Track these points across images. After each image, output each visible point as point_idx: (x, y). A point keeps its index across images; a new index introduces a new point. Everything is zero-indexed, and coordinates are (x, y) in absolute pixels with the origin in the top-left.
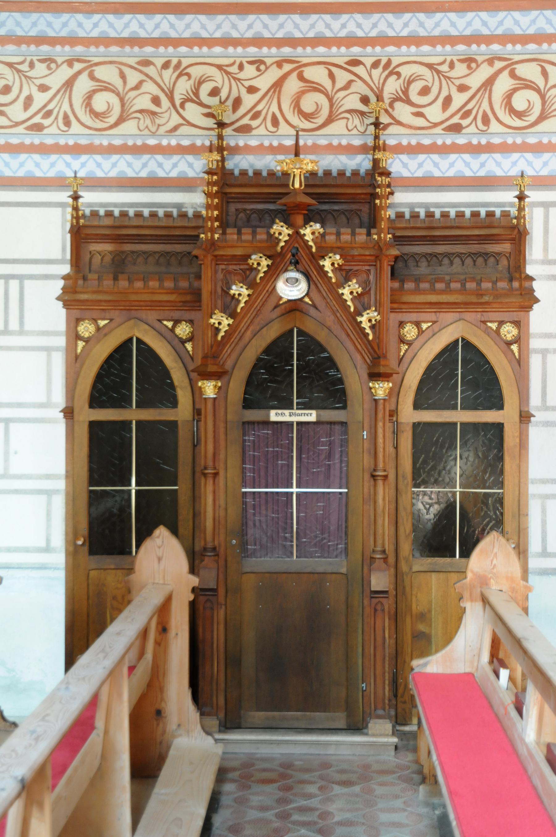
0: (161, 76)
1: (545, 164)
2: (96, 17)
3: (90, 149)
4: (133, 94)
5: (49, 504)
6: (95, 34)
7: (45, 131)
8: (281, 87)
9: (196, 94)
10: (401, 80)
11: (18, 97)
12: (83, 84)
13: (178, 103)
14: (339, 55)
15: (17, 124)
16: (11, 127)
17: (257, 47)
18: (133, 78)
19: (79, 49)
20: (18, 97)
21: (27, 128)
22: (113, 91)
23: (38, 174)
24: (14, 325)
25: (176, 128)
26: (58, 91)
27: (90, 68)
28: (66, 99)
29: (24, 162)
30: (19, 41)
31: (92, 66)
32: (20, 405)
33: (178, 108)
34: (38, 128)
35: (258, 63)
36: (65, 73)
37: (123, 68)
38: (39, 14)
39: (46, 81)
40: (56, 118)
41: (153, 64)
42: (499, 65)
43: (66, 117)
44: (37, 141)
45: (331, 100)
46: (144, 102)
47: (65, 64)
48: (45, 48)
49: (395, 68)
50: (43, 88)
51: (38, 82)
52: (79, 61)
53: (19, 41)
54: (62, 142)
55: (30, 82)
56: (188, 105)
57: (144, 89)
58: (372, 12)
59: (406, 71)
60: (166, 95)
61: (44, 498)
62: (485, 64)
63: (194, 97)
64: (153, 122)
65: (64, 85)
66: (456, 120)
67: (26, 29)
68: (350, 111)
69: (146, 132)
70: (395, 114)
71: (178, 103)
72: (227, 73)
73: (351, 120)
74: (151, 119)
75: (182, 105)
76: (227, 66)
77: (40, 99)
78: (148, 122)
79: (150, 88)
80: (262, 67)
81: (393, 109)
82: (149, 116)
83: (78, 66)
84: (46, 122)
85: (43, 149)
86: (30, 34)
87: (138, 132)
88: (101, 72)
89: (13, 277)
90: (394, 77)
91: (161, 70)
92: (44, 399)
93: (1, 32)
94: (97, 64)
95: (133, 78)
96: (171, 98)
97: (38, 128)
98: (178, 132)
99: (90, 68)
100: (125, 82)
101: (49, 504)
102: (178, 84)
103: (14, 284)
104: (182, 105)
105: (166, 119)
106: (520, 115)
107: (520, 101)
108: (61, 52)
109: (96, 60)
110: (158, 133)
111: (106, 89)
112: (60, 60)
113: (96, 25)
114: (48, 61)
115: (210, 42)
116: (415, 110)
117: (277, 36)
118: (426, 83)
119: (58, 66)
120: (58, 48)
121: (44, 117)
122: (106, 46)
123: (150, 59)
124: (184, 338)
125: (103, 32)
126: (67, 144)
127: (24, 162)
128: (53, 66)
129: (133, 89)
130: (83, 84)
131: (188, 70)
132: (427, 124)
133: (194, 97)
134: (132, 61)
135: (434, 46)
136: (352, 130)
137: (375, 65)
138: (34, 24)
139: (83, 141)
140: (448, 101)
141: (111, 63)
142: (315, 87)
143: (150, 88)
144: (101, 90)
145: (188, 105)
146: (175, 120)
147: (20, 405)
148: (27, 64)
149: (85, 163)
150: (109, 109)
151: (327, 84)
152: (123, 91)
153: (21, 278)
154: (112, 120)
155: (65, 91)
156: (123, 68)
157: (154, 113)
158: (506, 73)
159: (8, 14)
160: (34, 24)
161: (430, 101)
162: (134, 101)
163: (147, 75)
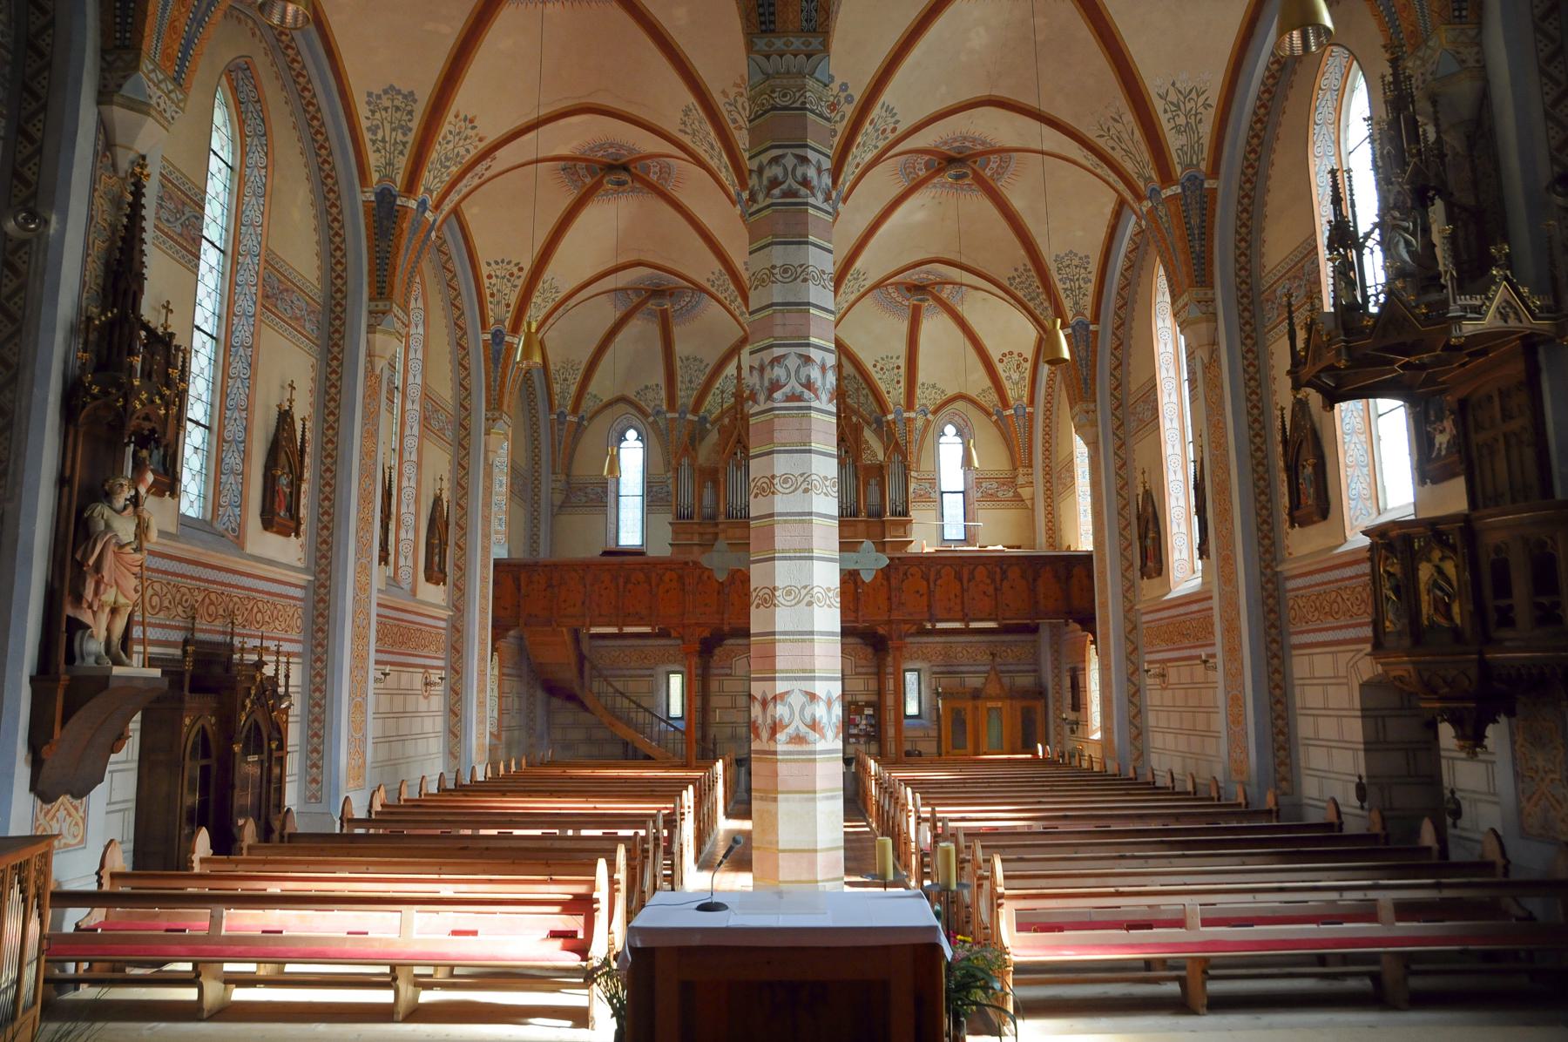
14: (220, 588)
142: (212, 603)
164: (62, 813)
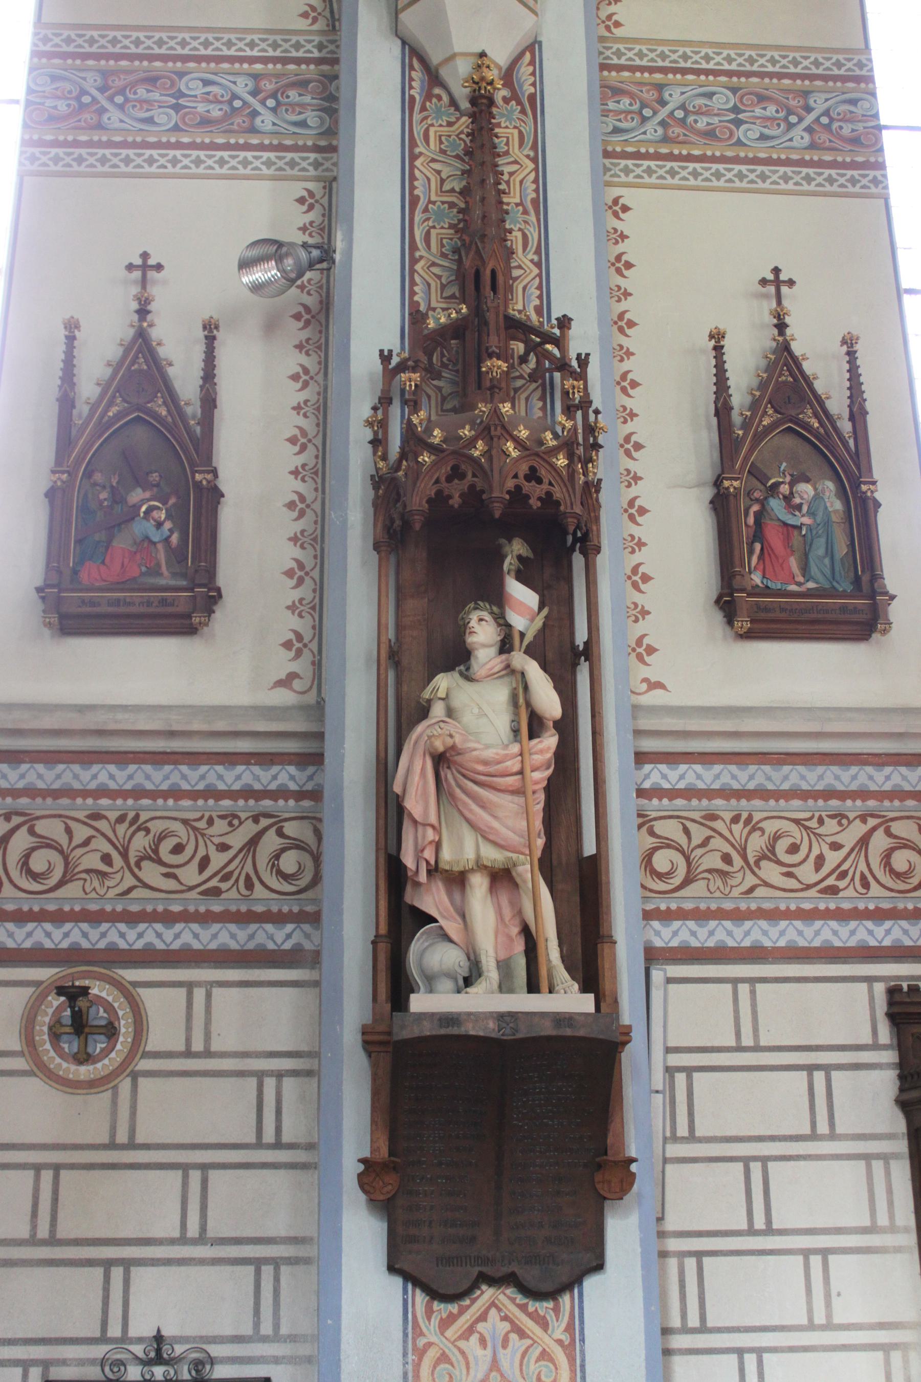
0: (114, 831)
2: (888, 770)
3: (893, 914)
5: (887, 1363)
6: (888, 787)
7: (841, 894)
8: (7, 843)
9: (156, 851)
10: (151, 836)
11: (808, 856)
12: (879, 842)
13: (752, 861)
15: (809, 887)
16: (802, 890)
18: (81, 833)
19: (871, 803)
20: (808, 856)
21: (820, 892)
22: (56, 849)
24: (823, 1128)
25: (751, 890)
26: (852, 850)
27: (886, 824)
28: (862, 858)
29: (819, 930)
30: (805, 795)
31: (887, 821)
32: (838, 1231)
33: (134, 867)
34: (833, 891)
35: (231, 818)
36: (858, 830)
37: (69, 822)
38: (825, 767)
39: (838, 839)
40: (853, 879)
41: (106, 818)
42: (16, 820)
43: (248, 877)
44: (832, 906)
45: (66, 859)
46: (93, 861)
47: (858, 820)
48: (834, 803)
49: (758, 823)
50: (836, 846)
51: (829, 840)
52: (872, 816)
53: (805, 795)
54: (861, 906)
55: (208, 842)
56: (763, 863)
57: (94, 845)
58: (712, 763)
59: (157, 827)
60: (738, 852)
61: (880, 1355)
62: (858, 821)
63: (769, 854)
64: (725, 883)
65: (858, 842)
66: (214, 883)
67: (812, 783)
70: (760, 873)
71: (132, 861)
72: (807, 828)
73: (712, 881)
75: (757, 863)
76: (195, 820)
77: (833, 858)
78: (719, 883)
79: (717, 843)
80: (844, 821)
81: (140, 868)
83: (872, 822)
84: (842, 884)
85: (841, 915)
86: (817, 788)
87: (83, 895)
88: (41, 827)
89: (818, 1067)
90: (143, 833)
92: (867, 1223)
95: (81, 833)
96: (125, 855)
97: (833, 891)
98: (131, 895)
99: (886, 824)
100: (71, 839)
101: (887, 1363)
102: (133, 841)
103: (819, 1076)
104: (757, 863)
105: (740, 879)
106: (35, 876)
107: (38, 863)
108: (853, 807)
109: (892, 815)
110: (107, 896)
111: (905, 846)
112: (851, 816)
113: (888, 778)
114: (839, 816)
115: (778, 795)
116: (165, 870)
117: (161, 788)
118: (178, 840)
119: (850, 822)
120: (849, 803)
121: (838, 879)
122: (902, 800)
123: (104, 813)
125: (895, 785)
126: (238, 911)
127: (819, 930)
128: (844, 821)
129: (699, 846)
130: (879, 842)
131: (149, 825)
132: (797, 886)
133: (769, 854)
134: (696, 815)
135: (155, 800)
137: (121, 819)
138: (821, 777)
139: (886, 905)
140: (204, 863)
141: (908, 818)
143: (717, 843)
144: (900, 848)
145: (145, 864)
146: (130, 881)
147: (838, 1231)
148: (815, 819)
149: (890, 929)
150: (50, 870)
151: (683, 840)
153: (827, 1069)
154: (677, 881)
155: (860, 849)
156: (69, 822)
157: (104, 875)
158: (24, 829)
159: (791, 767)
160: (821, 777)
161: (187, 859)
163: (97, 830)
164: (495, 1326)
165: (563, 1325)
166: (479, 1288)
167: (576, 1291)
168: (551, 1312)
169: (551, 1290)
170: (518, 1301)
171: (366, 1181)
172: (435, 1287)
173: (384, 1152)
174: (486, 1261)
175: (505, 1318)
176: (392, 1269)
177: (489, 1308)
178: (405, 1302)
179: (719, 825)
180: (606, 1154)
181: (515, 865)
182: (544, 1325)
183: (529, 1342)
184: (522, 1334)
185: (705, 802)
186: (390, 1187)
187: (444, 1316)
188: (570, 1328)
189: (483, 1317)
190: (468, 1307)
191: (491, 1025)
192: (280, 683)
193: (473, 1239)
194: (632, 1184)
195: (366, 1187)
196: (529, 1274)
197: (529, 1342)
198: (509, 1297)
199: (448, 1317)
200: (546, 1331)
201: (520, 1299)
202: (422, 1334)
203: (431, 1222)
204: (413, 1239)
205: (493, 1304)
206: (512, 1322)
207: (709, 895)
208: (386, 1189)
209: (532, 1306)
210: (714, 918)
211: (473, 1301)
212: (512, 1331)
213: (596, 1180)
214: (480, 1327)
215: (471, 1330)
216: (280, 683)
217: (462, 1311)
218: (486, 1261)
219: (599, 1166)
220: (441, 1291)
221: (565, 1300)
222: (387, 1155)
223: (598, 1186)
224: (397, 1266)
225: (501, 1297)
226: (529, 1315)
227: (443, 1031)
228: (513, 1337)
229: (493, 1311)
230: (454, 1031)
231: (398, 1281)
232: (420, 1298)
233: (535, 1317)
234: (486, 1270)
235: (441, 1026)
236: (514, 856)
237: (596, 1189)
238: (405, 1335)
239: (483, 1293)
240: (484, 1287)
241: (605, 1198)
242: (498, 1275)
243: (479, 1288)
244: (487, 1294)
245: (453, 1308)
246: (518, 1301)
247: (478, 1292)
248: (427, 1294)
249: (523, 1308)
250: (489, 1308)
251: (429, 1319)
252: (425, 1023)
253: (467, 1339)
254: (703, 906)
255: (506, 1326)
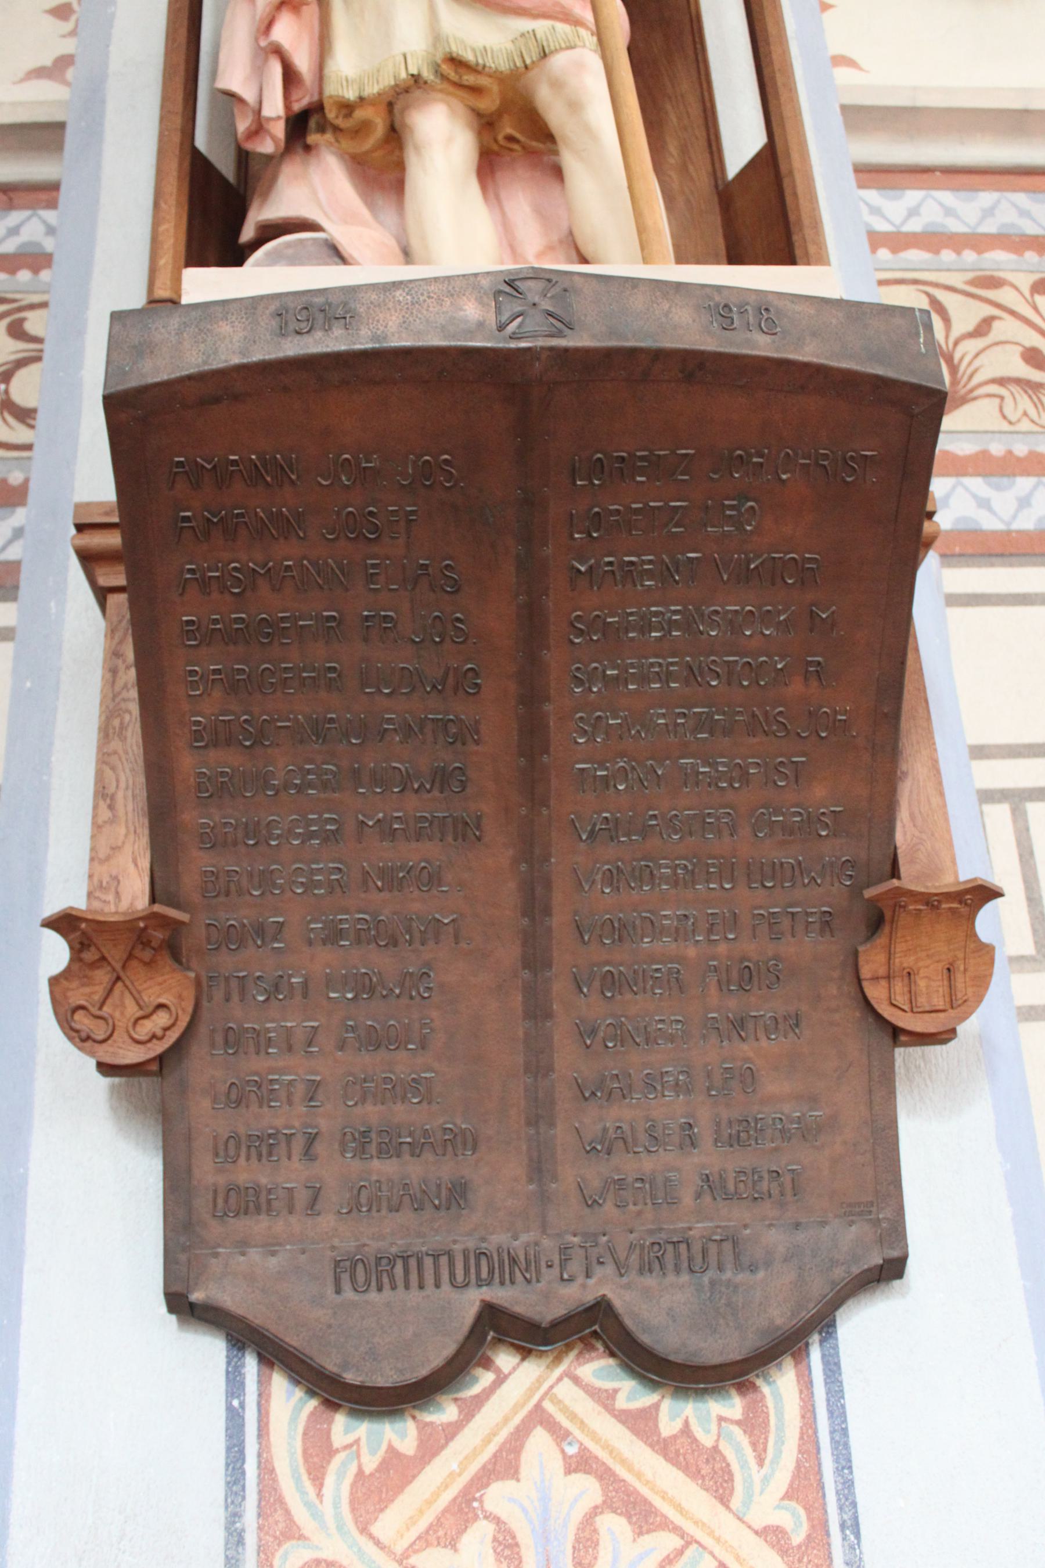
1: (1024, 502)
4: (970, 346)
17: (929, 250)
23: (989, 523)
31: (20, 309)
68: (1001, 381)
69: (1025, 425)
74: (1030, 397)
79: (1005, 328)
82: (1026, 392)
91: (1032, 295)
93: (9, 247)
94: (32, 307)
124: (159, 958)
134: (956, 280)
136: (1019, 421)
152: (947, 337)
162: (977, 363)
164: (544, 1494)
165: (783, 1476)
166: (487, 1363)
167: (815, 1355)
168: (737, 1431)
169: (735, 1354)
170: (622, 1402)
171: (77, 998)
172: (330, 1364)
173: (134, 894)
174: (510, 1266)
175: (581, 1463)
176: (182, 1305)
177: (521, 1433)
178: (235, 1419)
179: (1005, 296)
180: (895, 872)
181: (544, 55)
182: (719, 1481)
183: (668, 1542)
184: (643, 1516)
185: (969, 256)
186: (162, 1018)
187: (370, 1463)
188: (805, 1486)
189: (505, 1464)
190: (452, 1431)
191: (472, 311)
192: (39, 73)
193: (458, 1194)
194: (982, 982)
195: (82, 1021)
196: (657, 1307)
197: (668, 1542)
198: (593, 1393)
199: (384, 1466)
200: (724, 1500)
201: (630, 1393)
202: (292, 1532)
203: (312, 1139)
204: (249, 1202)
205: (538, 1417)
206: (605, 1475)
207: (1006, 427)
208: (147, 1028)
209: (674, 1413)
210: (1026, 473)
211: (470, 1409)
212: (608, 1505)
213: (865, 972)
214: (498, 1497)
215: (464, 1509)
216: (39, 73)
217: (431, 1446)
218: (510, 1266)
219: (876, 921)
220: (350, 1377)
221: (781, 1386)
222: (142, 903)
223: (876, 993)
224: (197, 1296)
225: (566, 1390)
226: (664, 1448)
227: (292, 348)
228: (614, 1526)
229: (539, 1440)
230: (332, 341)
231: (210, 1349)
232: (288, 1403)
233: (681, 1452)
234: (501, 1295)
235: (282, 332)
236: (541, 26)
237: (867, 1004)
238: (235, 1538)
239: (501, 1379)
240: (505, 1359)
241: (896, 1034)
242: (548, 1313)
243: (487, 1363)
244: (515, 1381)
245: (400, 1434)
246: (622, 1402)
247: (485, 1378)
248: (311, 1393)
249: (640, 1424)
250: (521, 1433)
251: (317, 1477)
252: (225, 328)
253: (453, 1544)
254: (997, 449)
255: (587, 1490)
